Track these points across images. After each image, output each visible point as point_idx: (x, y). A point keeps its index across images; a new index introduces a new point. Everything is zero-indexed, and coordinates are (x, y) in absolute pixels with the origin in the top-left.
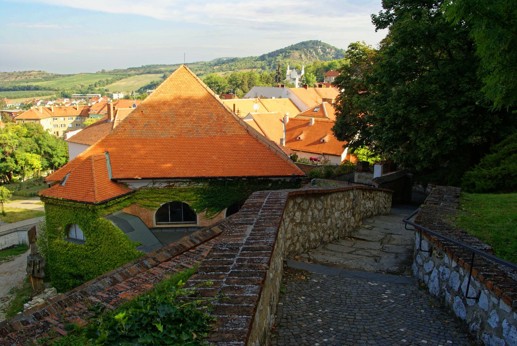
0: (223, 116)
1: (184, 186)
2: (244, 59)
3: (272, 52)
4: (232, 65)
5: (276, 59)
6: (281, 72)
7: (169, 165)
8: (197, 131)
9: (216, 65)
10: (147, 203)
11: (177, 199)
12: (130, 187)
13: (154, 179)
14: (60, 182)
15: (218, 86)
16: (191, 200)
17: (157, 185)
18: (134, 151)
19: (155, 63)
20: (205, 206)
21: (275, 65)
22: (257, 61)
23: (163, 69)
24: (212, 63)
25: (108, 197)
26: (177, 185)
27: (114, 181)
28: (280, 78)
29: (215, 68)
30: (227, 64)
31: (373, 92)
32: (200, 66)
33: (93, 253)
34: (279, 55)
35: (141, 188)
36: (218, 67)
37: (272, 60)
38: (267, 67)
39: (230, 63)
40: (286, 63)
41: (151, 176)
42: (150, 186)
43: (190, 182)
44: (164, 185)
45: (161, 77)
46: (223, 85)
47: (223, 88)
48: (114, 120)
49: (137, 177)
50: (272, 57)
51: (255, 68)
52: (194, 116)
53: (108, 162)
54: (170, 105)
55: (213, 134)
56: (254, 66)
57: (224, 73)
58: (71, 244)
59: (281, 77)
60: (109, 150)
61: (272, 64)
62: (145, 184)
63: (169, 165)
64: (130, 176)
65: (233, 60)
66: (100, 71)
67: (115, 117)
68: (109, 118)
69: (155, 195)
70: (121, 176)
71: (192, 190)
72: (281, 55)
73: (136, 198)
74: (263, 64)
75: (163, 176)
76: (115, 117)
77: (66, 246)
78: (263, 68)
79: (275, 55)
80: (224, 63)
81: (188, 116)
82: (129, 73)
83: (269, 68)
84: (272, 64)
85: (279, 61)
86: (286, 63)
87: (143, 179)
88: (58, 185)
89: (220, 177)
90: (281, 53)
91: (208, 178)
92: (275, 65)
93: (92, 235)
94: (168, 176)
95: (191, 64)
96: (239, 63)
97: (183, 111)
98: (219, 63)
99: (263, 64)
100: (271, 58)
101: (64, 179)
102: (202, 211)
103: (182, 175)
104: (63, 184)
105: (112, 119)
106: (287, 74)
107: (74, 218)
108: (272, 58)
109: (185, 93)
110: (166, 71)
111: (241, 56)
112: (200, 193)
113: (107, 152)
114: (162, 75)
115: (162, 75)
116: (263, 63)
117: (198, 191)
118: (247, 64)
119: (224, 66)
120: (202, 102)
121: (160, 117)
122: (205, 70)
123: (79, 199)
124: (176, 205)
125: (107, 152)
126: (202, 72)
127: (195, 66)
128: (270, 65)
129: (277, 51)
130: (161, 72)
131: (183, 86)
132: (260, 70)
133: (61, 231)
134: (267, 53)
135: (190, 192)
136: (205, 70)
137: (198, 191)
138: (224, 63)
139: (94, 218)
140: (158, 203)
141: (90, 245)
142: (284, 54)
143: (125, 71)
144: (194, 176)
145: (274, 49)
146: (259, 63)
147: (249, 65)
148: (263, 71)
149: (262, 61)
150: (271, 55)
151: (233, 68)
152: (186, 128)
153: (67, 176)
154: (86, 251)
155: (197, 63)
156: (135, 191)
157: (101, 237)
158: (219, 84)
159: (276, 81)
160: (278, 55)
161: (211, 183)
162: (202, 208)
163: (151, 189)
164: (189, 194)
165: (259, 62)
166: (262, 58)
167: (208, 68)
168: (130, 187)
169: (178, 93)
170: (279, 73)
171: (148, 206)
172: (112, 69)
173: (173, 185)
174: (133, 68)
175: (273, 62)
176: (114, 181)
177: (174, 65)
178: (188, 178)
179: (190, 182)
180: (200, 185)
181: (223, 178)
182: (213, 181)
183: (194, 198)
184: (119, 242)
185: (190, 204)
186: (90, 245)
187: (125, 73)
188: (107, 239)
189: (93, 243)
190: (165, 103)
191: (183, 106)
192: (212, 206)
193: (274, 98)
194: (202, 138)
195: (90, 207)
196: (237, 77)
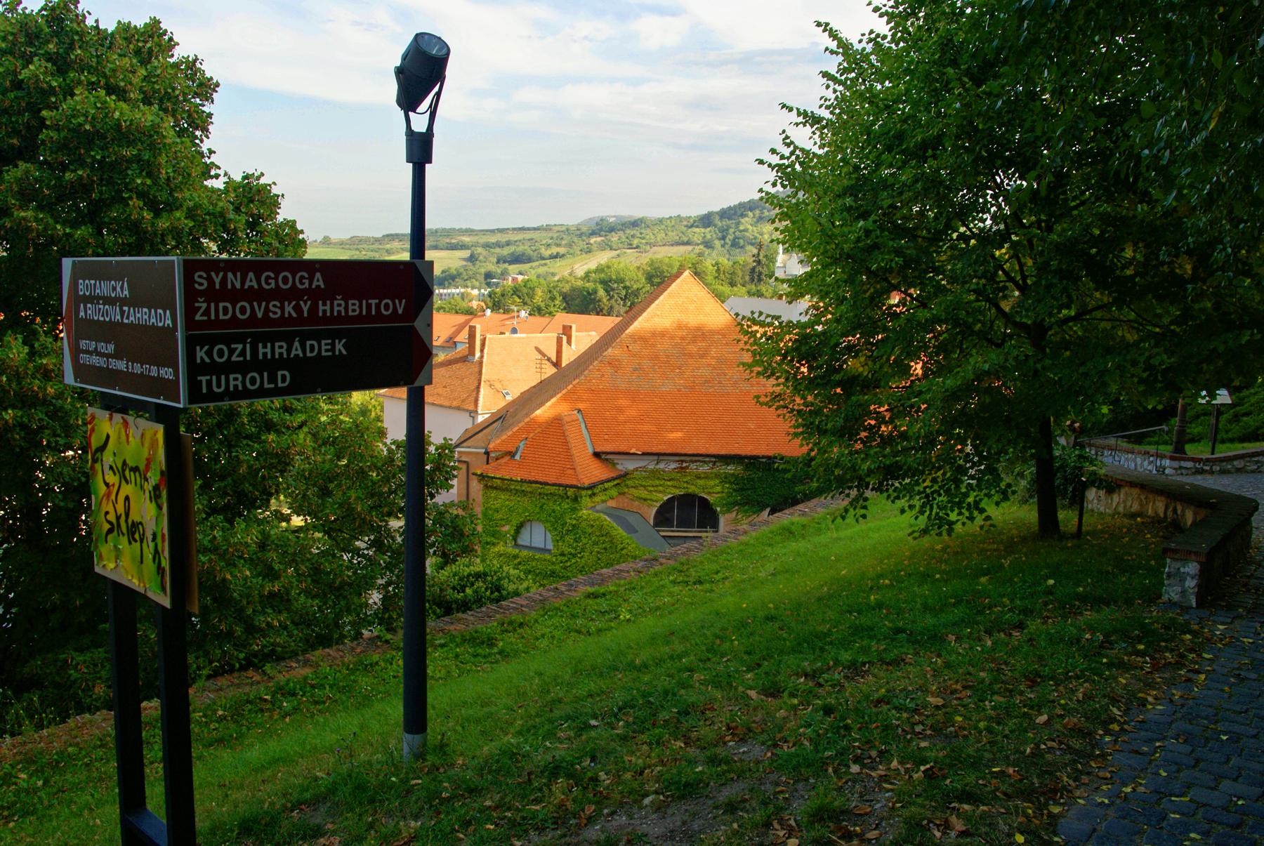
1: (705, 468)
2: (661, 221)
3: (730, 208)
5: (738, 224)
6: (764, 261)
7: (679, 434)
8: (720, 382)
9: (593, 233)
10: (644, 494)
11: (692, 489)
12: (619, 467)
13: (659, 455)
14: (512, 454)
15: (625, 287)
16: (714, 492)
17: (661, 466)
18: (620, 410)
19: (448, 225)
20: (735, 504)
21: (736, 238)
22: (692, 226)
23: (466, 239)
24: (584, 229)
25: (594, 480)
26: (693, 466)
27: (597, 455)
28: (760, 274)
29: (592, 240)
31: (881, 184)
33: (565, 568)
34: (746, 216)
35: (636, 469)
36: (599, 239)
37: (729, 227)
38: (718, 243)
39: (628, 231)
41: (654, 450)
42: (651, 467)
43: (714, 463)
44: (673, 466)
45: (465, 259)
46: (635, 287)
48: (482, 357)
49: (633, 451)
50: (729, 219)
51: (688, 243)
52: (713, 358)
53: (583, 426)
54: (672, 338)
56: (685, 239)
57: (614, 253)
58: (525, 553)
59: (765, 271)
60: (581, 406)
61: (731, 237)
62: (642, 464)
63: (679, 434)
64: (622, 448)
65: (635, 224)
66: (320, 239)
67: (482, 351)
68: (472, 353)
69: (657, 482)
70: (608, 448)
71: (717, 476)
72: (750, 214)
73: (627, 486)
74: (708, 236)
75: (674, 451)
76: (482, 351)
77: (515, 557)
78: (708, 244)
79: (735, 214)
80: (612, 230)
81: (702, 356)
82: (388, 246)
83: (723, 246)
85: (746, 230)
86: (762, 234)
87: (644, 454)
88: (506, 459)
89: (763, 457)
90: (751, 209)
92: (736, 238)
93: (567, 538)
94: (683, 452)
95: (535, 229)
96: (648, 231)
97: (693, 348)
98: (601, 230)
99: (708, 236)
100: (726, 222)
101: (517, 449)
102: (729, 511)
103: (703, 451)
104: (517, 457)
105: (478, 354)
106: (778, 264)
107: (537, 510)
109: (693, 320)
110: (476, 245)
111: (653, 213)
112: (731, 483)
113: (579, 411)
114: (466, 253)
115: (466, 253)
116: (709, 233)
117: (725, 479)
119: (614, 238)
120: (724, 335)
121: (657, 358)
122: (570, 245)
123: (552, 480)
124: (688, 501)
125: (579, 411)
126: (562, 250)
127: (544, 234)
128: (724, 238)
129: (741, 205)
130: (462, 247)
131: (691, 307)
133: (507, 533)
134: (717, 209)
135: (712, 479)
136: (570, 245)
137: (725, 479)
138: (612, 230)
139: (574, 510)
140: (660, 495)
141: (562, 554)
142: (757, 212)
143: (377, 240)
144: (723, 453)
145: (733, 201)
146: (698, 233)
147: (673, 236)
148: (707, 251)
149: (705, 227)
150: (724, 214)
151: (635, 242)
152: (702, 376)
153: (522, 445)
154: (553, 563)
155: (548, 228)
156: (626, 474)
157: (584, 541)
158: (628, 284)
159: (752, 280)
160: (743, 216)
161: (747, 468)
162: (730, 506)
163: (653, 471)
164: (712, 483)
165: (697, 230)
166: (706, 220)
167: (575, 239)
168: (619, 467)
169: (684, 318)
170: (759, 262)
171: (645, 500)
172: (345, 236)
173: (687, 467)
174: (397, 235)
175: (732, 230)
176: (597, 455)
177: (493, 231)
178: (714, 456)
179: (714, 463)
180: (731, 469)
181: (769, 458)
182: (750, 462)
183: (719, 489)
184: (620, 546)
185: (711, 499)
186: (562, 554)
187: (376, 246)
188: (595, 543)
189: (567, 550)
190: (663, 334)
191: (694, 341)
192: (746, 504)
194: (728, 394)
195: (571, 492)
196: (665, 268)
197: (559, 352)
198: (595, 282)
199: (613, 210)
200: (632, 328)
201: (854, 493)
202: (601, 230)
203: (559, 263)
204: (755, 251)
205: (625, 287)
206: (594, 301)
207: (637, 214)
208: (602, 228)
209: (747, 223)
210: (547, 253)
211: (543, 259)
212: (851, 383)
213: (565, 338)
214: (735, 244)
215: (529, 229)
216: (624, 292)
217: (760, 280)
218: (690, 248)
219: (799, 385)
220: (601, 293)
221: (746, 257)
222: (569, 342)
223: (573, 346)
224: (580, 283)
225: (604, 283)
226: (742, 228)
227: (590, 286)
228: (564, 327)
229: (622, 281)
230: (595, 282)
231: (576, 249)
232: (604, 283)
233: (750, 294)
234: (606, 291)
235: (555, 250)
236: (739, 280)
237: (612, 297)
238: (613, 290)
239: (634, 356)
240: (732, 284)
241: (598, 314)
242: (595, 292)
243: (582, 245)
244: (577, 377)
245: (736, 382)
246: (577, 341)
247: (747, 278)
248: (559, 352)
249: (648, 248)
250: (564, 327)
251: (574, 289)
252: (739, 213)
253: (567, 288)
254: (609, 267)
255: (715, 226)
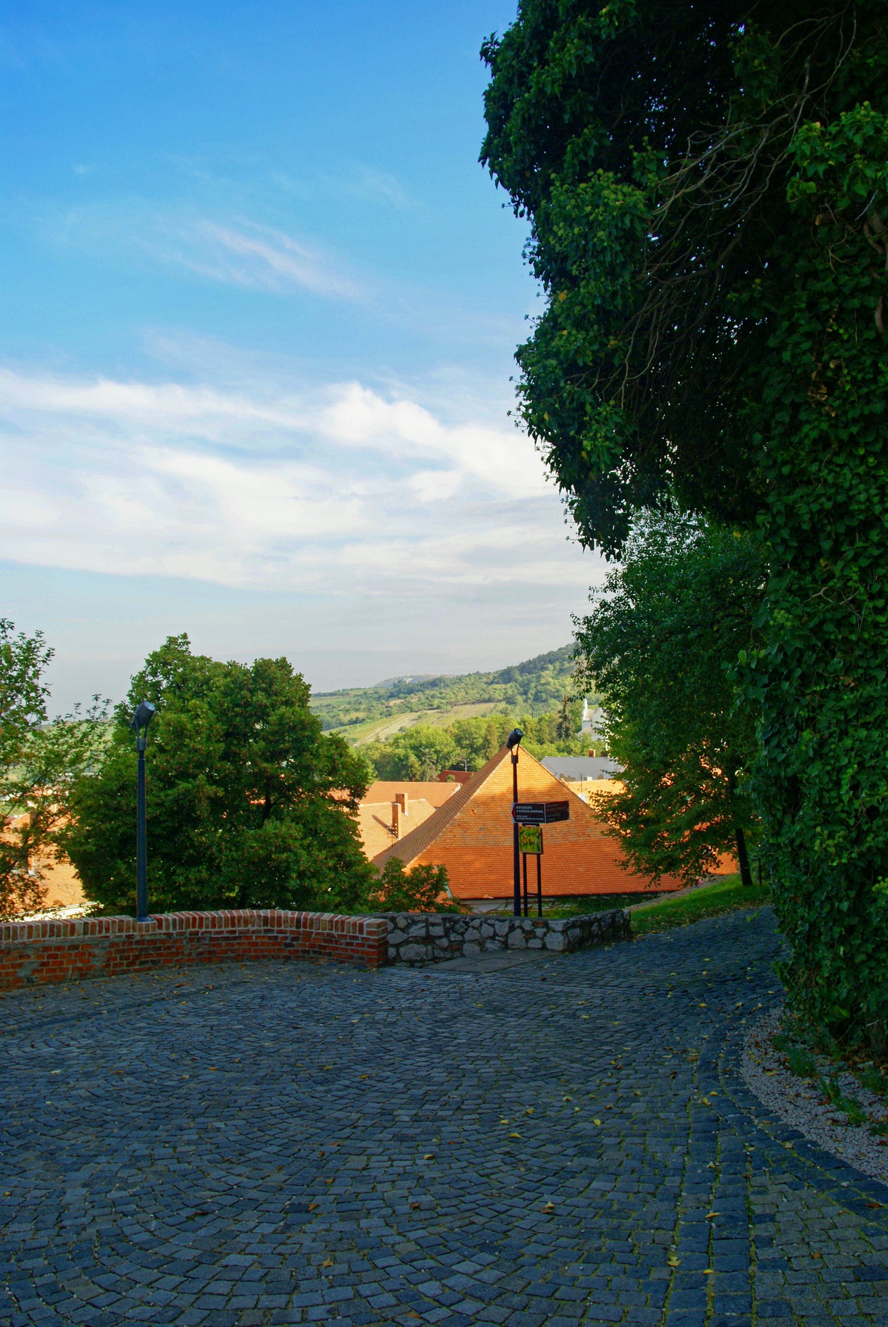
0: (583, 814)
2: (460, 679)
3: (529, 662)
4: (433, 697)
5: (539, 677)
6: (570, 715)
8: (552, 836)
9: (392, 696)
15: (436, 752)
22: (492, 683)
24: (382, 692)
28: (568, 729)
29: (392, 703)
30: (420, 694)
32: (353, 700)
34: (546, 669)
36: (398, 702)
37: (530, 681)
38: (520, 699)
39: (427, 692)
40: (564, 687)
41: (503, 894)
42: (501, 909)
43: (553, 903)
46: (446, 750)
47: (447, 757)
49: (486, 896)
50: (530, 673)
51: (489, 700)
55: (573, 838)
56: (486, 696)
57: (415, 715)
59: (572, 726)
61: (532, 691)
64: (477, 895)
65: (434, 683)
70: (465, 895)
72: (551, 667)
74: (510, 692)
78: (510, 700)
79: (535, 667)
80: (410, 691)
83: (525, 701)
84: (532, 691)
85: (548, 684)
86: (564, 687)
87: (495, 898)
91: (579, 896)
95: (331, 694)
96: (448, 690)
98: (399, 692)
99: (510, 692)
106: (584, 718)
108: (529, 676)
111: (450, 671)
116: (510, 688)
118: (470, 691)
119: (414, 699)
122: (369, 710)
126: (361, 715)
127: (341, 699)
129: (541, 658)
132: (502, 705)
134: (516, 663)
136: (369, 710)
142: (558, 664)
144: (560, 893)
145: (532, 656)
146: (498, 691)
147: (474, 693)
148: (510, 707)
149: (505, 683)
150: (525, 668)
151: (436, 702)
155: (344, 693)
158: (438, 748)
159: (560, 736)
160: (543, 669)
165: (498, 686)
166: (506, 676)
167: (374, 703)
175: (533, 685)
179: (553, 903)
180: (567, 907)
181: (598, 895)
193: (590, 779)
196: (473, 730)
197: (395, 819)
198: (405, 747)
199: (410, 671)
200: (475, 794)
201: (653, 874)
202: (399, 692)
203: (359, 728)
204: (561, 707)
205: (436, 752)
206: (405, 767)
207: (434, 673)
208: (401, 690)
209: (547, 675)
210: (346, 719)
211: (342, 724)
212: (647, 821)
213: (399, 805)
214: (537, 698)
215: (325, 695)
216: (435, 757)
217: (567, 736)
218: (492, 705)
219: (624, 825)
220: (413, 758)
221: (553, 710)
222: (403, 810)
223: (406, 813)
224: (389, 750)
225: (416, 748)
226: (543, 681)
227: (401, 752)
228: (397, 796)
229: (432, 745)
230: (405, 747)
231: (376, 713)
232: (416, 748)
233: (559, 750)
234: (417, 756)
235: (354, 715)
236: (547, 737)
237: (423, 763)
238: (424, 754)
239: (479, 818)
240: (541, 742)
241: (411, 780)
242: (407, 757)
243: (382, 708)
244: (432, 838)
245: (565, 835)
246: (410, 808)
247: (555, 734)
248: (395, 819)
249: (449, 707)
250: (397, 796)
251: (384, 756)
252: (539, 666)
253: (376, 755)
254: (418, 732)
255: (516, 681)
